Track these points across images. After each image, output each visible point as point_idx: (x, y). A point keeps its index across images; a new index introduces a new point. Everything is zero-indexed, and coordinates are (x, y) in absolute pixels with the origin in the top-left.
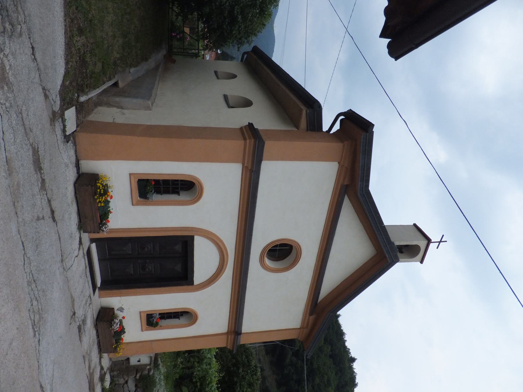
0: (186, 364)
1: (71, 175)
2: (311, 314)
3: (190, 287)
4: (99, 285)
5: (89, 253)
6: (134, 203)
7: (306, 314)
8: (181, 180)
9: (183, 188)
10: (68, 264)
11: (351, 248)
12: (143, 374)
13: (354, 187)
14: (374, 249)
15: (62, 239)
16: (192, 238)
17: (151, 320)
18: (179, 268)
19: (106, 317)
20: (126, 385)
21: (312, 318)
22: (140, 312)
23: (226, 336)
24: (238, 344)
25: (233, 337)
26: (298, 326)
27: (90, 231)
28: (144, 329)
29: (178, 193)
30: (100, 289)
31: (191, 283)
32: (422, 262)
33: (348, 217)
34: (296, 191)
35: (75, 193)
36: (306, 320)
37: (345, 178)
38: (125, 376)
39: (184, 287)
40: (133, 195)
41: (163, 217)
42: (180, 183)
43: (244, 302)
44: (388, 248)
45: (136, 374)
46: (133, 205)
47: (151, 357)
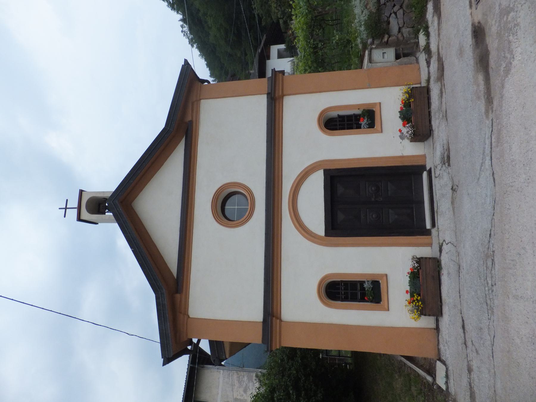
0: (330, 56)
1: (445, 320)
2: (191, 122)
3: (328, 167)
4: (425, 174)
5: (433, 225)
6: (385, 278)
7: (196, 121)
8: (336, 129)
9: (339, 291)
10: (457, 223)
11: (160, 206)
12: (380, 40)
13: (169, 285)
14: (135, 208)
15: (460, 324)
16: (327, 234)
17: (370, 122)
18: (340, 190)
19: (421, 132)
20: (401, 26)
21: (189, 118)
22: (382, 132)
23: (285, 93)
24: (276, 346)
25: (277, 95)
26: (202, 101)
27: (430, 261)
28: (378, 106)
29: (339, 116)
30: (423, 168)
31: (327, 172)
32: (81, 192)
33: (170, 251)
34: (226, 288)
35: (441, 306)
36: (194, 114)
37: (181, 301)
38: (401, 38)
39: (334, 168)
40: (385, 284)
41: (357, 259)
42: (338, 127)
43: (267, 142)
44: (120, 205)
45: (388, 40)
46: (386, 275)
47: (370, 61)
